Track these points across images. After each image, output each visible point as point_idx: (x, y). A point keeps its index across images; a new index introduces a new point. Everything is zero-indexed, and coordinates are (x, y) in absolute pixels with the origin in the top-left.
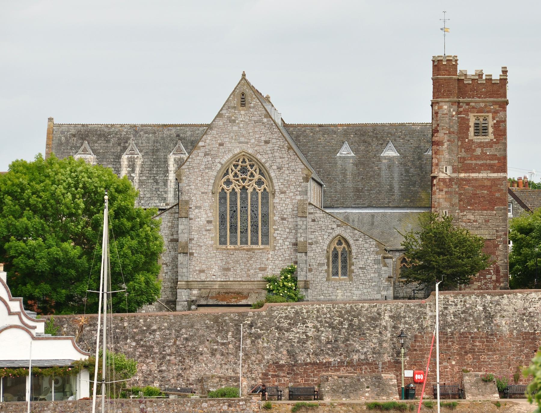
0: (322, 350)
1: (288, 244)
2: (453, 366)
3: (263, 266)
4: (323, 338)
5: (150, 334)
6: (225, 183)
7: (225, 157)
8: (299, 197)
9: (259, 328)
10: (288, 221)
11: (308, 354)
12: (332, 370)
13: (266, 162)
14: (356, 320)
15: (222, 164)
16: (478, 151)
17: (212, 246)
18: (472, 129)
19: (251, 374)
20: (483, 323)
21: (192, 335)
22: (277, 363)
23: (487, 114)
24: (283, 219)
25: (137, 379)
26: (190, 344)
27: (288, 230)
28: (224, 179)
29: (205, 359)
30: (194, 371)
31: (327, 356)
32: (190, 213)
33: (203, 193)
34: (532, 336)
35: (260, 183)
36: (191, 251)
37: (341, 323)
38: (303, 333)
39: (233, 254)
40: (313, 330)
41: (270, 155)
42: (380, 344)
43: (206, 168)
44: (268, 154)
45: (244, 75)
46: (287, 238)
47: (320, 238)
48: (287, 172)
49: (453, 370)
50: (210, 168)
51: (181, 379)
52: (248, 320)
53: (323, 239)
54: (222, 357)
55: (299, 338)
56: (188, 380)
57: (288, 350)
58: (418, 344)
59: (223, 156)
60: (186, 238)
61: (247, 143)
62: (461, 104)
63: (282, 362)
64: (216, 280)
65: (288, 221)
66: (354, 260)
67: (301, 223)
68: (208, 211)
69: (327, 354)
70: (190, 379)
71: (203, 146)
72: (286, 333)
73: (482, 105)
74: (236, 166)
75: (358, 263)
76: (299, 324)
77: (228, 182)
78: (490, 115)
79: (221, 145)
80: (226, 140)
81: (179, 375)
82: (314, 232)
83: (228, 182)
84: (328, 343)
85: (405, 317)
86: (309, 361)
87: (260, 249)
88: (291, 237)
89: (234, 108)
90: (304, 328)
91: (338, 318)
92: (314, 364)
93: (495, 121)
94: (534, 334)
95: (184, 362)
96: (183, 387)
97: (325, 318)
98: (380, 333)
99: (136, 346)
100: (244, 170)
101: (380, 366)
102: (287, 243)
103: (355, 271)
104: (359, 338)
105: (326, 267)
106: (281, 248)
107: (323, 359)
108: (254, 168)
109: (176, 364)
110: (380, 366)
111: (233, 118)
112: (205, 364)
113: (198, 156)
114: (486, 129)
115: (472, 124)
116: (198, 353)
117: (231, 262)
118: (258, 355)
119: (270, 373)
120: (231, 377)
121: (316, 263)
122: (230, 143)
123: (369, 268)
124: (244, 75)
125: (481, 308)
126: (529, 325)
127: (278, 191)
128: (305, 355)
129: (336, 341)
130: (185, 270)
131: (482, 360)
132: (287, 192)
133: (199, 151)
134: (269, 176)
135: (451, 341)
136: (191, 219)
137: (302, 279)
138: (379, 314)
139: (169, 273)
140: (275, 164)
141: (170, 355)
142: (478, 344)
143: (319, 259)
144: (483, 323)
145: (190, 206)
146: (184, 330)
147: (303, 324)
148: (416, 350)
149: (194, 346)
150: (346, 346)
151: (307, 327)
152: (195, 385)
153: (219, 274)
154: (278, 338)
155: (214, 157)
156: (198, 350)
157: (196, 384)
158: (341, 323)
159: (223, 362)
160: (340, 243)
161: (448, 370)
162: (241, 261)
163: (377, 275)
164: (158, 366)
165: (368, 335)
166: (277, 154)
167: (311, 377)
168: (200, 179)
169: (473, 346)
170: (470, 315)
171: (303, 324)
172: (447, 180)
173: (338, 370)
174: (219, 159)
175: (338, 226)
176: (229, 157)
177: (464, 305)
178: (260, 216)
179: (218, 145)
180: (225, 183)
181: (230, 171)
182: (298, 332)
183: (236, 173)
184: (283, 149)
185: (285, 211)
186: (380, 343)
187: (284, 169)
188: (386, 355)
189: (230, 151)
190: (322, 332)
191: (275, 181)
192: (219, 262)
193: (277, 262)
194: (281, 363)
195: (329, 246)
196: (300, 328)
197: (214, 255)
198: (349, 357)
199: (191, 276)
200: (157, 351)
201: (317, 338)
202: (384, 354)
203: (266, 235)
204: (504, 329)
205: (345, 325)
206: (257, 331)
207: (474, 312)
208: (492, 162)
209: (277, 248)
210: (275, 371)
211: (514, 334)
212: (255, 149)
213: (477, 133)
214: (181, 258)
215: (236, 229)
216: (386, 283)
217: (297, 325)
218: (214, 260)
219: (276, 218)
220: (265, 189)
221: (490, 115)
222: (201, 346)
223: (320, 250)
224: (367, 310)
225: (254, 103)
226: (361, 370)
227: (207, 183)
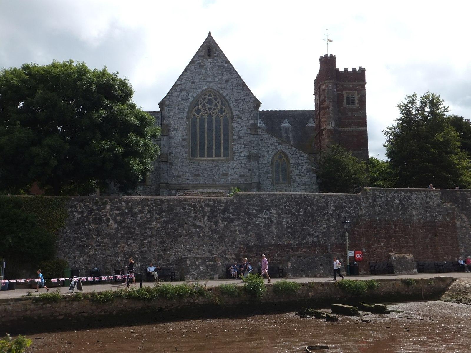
0: (284, 234)
1: (244, 156)
2: (382, 247)
3: (224, 172)
4: (284, 223)
5: (132, 216)
6: (196, 111)
7: (196, 92)
8: (251, 121)
9: (231, 213)
10: (243, 139)
11: (273, 237)
12: (292, 250)
13: (227, 95)
14: (309, 208)
15: (194, 97)
16: (350, 114)
17: (186, 158)
18: (345, 101)
19: (225, 254)
20: (401, 213)
21: (172, 218)
22: (247, 244)
23: (353, 92)
24: (240, 137)
25: (119, 259)
26: (170, 227)
27: (243, 146)
28: (196, 108)
29: (184, 240)
30: (174, 251)
31: (288, 239)
32: (170, 133)
33: (179, 118)
34: (433, 224)
35: (221, 111)
36: (170, 162)
37: (298, 211)
38: (268, 219)
39: (202, 164)
40: (276, 216)
41: (230, 91)
42: (328, 229)
43: (181, 100)
44: (228, 90)
45: (210, 33)
46: (243, 151)
47: (266, 153)
48: (242, 103)
49: (382, 250)
50: (185, 100)
51: (162, 260)
52: (221, 206)
53: (269, 154)
54: (199, 239)
55: (265, 222)
56: (168, 260)
57: (256, 234)
58: (356, 229)
59: (195, 92)
60: (166, 151)
61: (212, 82)
62: (338, 86)
63: (251, 244)
64: (189, 183)
65: (243, 139)
66: (292, 169)
67: (254, 139)
68: (183, 132)
69: (288, 237)
70: (170, 259)
71: (180, 84)
72: (254, 218)
73: (351, 86)
74: (204, 99)
75: (295, 171)
76: (265, 210)
77: (198, 111)
78: (356, 92)
79: (193, 83)
80: (197, 79)
81: (160, 255)
82: (261, 148)
83: (198, 111)
84: (289, 227)
85: (345, 207)
86: (273, 243)
87: (222, 160)
88: (246, 151)
89: (203, 56)
90: (269, 214)
91: (295, 207)
92: (278, 245)
93: (359, 96)
94: (434, 222)
95: (164, 243)
96: (163, 267)
97: (285, 206)
98: (328, 220)
99: (117, 228)
100: (210, 102)
101: (329, 247)
102: (242, 155)
103: (293, 177)
104: (312, 224)
105: (271, 175)
106: (238, 159)
107: (284, 241)
108: (217, 100)
109: (156, 246)
110: (329, 247)
111: (202, 64)
112: (184, 245)
113: (176, 91)
114: (354, 101)
115: (345, 97)
116: (177, 235)
117: (200, 169)
118: (231, 238)
119: (242, 254)
120: (207, 258)
121: (263, 171)
122: (200, 82)
123: (303, 174)
124: (210, 33)
125: (398, 202)
126: (430, 216)
127: (236, 116)
128: (270, 238)
129: (295, 226)
130: (165, 175)
131: (401, 242)
132: (243, 117)
133: (177, 88)
134: (230, 106)
135: (379, 227)
136: (170, 138)
137: (255, 181)
138: (326, 204)
139: (154, 179)
140: (233, 97)
141: (151, 237)
142: (398, 229)
143: (266, 168)
144: (401, 213)
145: (170, 128)
146: (164, 214)
147: (268, 211)
148: (355, 234)
149: (174, 228)
150: (302, 230)
151: (271, 213)
152: (174, 265)
153: (192, 178)
154: (248, 222)
155: (188, 92)
156: (178, 232)
157: (176, 265)
158: (298, 211)
159: (200, 244)
160: (281, 157)
161: (378, 250)
162: (208, 169)
163: (309, 180)
164: (139, 247)
165: (319, 221)
166: (234, 90)
167: (276, 257)
168: (177, 108)
169: (395, 231)
170: (392, 207)
171: (268, 211)
172: (333, 131)
173: (297, 251)
174: (191, 94)
175: (279, 144)
176: (199, 92)
177: (387, 199)
178: (222, 136)
179: (191, 84)
180: (196, 111)
181: (199, 102)
182: (264, 218)
183: (204, 104)
184: (239, 86)
185: (241, 131)
186: (329, 227)
187: (240, 100)
188: (333, 238)
189: (199, 87)
190: (283, 219)
191: (233, 109)
192: (192, 169)
193: (235, 169)
194: (250, 244)
195: (273, 159)
196: (266, 214)
197: (188, 164)
198: (305, 240)
199: (170, 180)
200: (138, 232)
201: (279, 223)
202: (332, 237)
203: (226, 149)
204: (415, 218)
205: (301, 212)
206: (230, 216)
207: (394, 204)
208: (358, 121)
209: (235, 159)
210: (245, 252)
211: (422, 222)
212: (218, 86)
213: (348, 103)
214: (163, 165)
215: (204, 146)
216: (315, 186)
217: (263, 212)
218: (188, 168)
219: (234, 137)
220: (225, 116)
221: (356, 92)
222: (180, 229)
223: (267, 162)
224: (317, 200)
225: (218, 53)
226: (315, 250)
227: (183, 111)
